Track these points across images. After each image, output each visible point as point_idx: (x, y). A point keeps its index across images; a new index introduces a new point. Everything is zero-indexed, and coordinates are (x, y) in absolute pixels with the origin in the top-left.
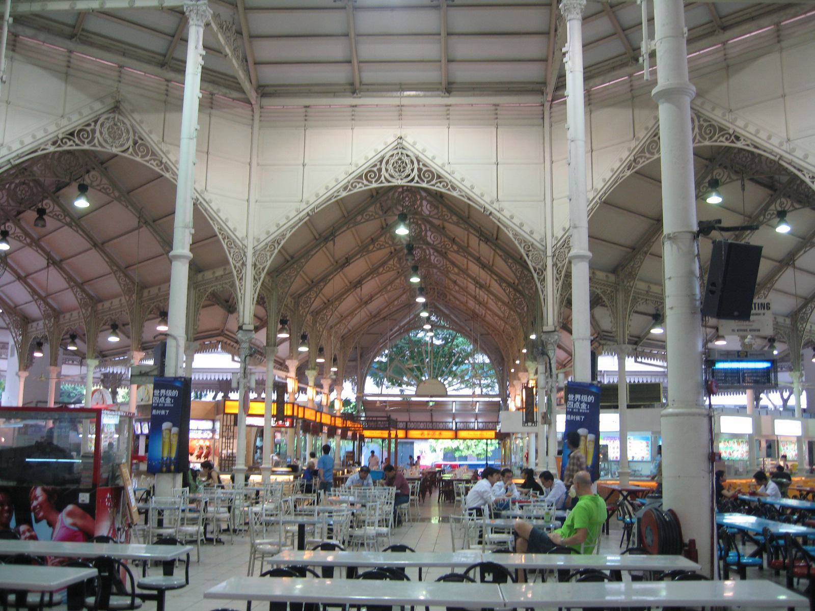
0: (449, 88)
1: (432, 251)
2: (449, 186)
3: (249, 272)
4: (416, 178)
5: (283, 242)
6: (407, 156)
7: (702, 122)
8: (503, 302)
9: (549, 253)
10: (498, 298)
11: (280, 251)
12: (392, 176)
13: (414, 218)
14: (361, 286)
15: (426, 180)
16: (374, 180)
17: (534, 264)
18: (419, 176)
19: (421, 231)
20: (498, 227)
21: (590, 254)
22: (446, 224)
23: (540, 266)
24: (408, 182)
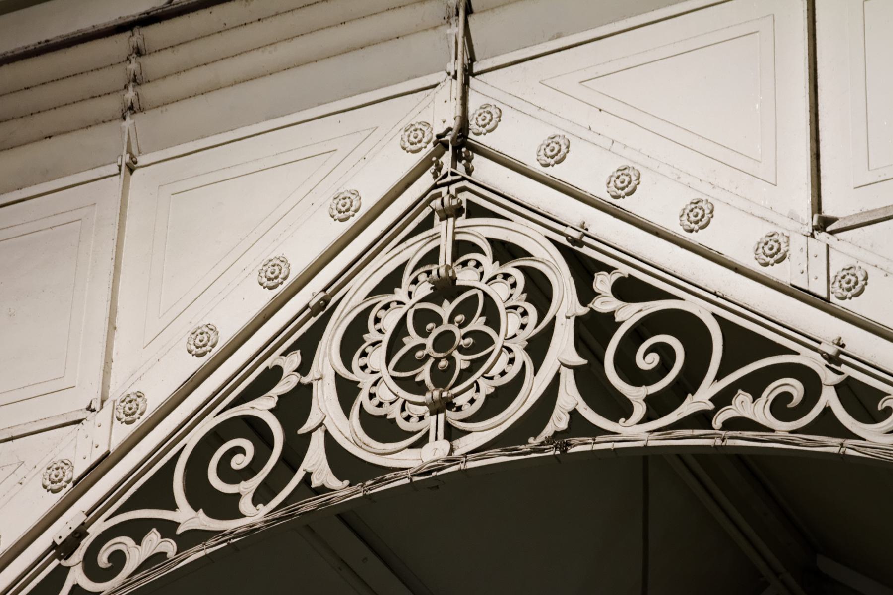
2: (829, 397)
6: (505, 251)
7: (605, 303)
12: (380, 428)
15: (637, 395)
16: (247, 488)
18: (590, 380)
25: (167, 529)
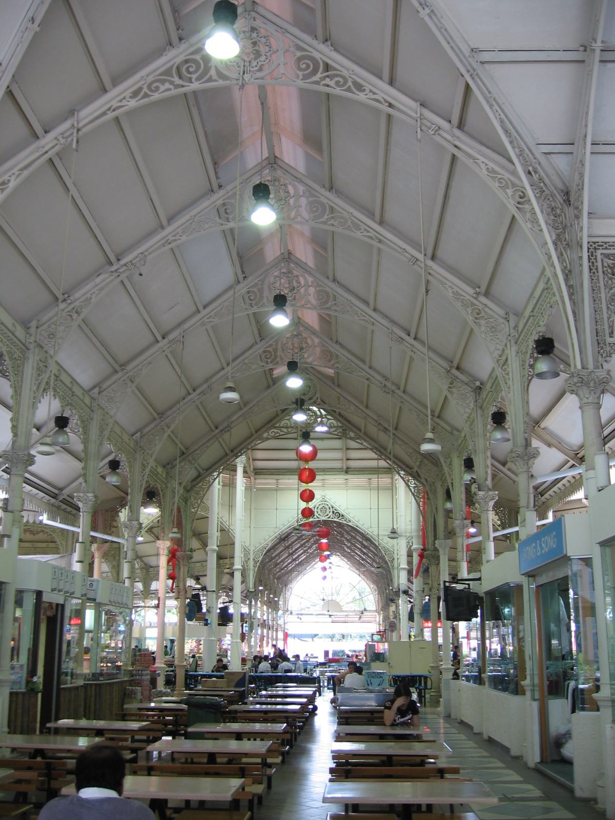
0: (347, 471)
2: (350, 83)
21: (407, 567)
25: (172, 83)
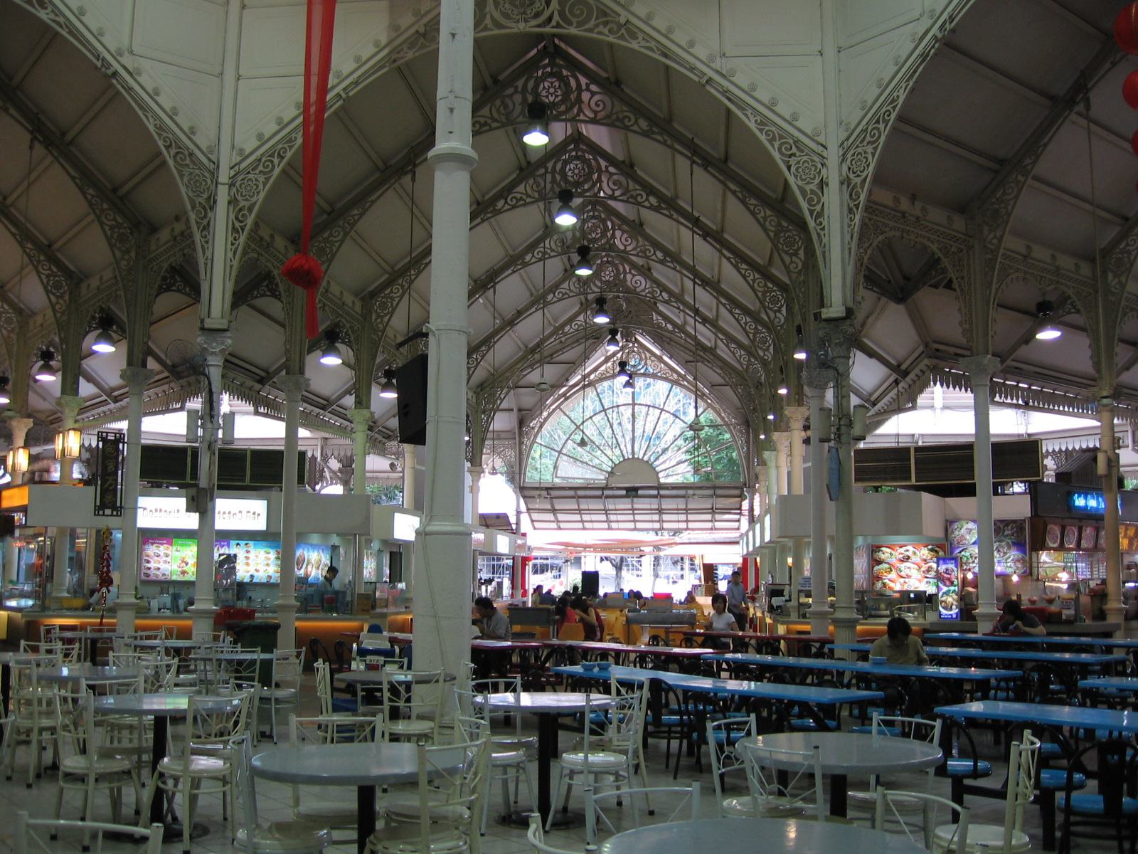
1: (583, 81)
3: (221, 217)
4: (556, 18)
5: (289, 155)
8: (740, 345)
9: (224, 177)
10: (730, 338)
11: (284, 171)
13: (608, 256)
14: (494, 287)
17: (800, 183)
18: (562, 14)
19: (618, 274)
20: (728, 111)
22: (652, 263)
23: (813, 187)
24: (539, 26)
